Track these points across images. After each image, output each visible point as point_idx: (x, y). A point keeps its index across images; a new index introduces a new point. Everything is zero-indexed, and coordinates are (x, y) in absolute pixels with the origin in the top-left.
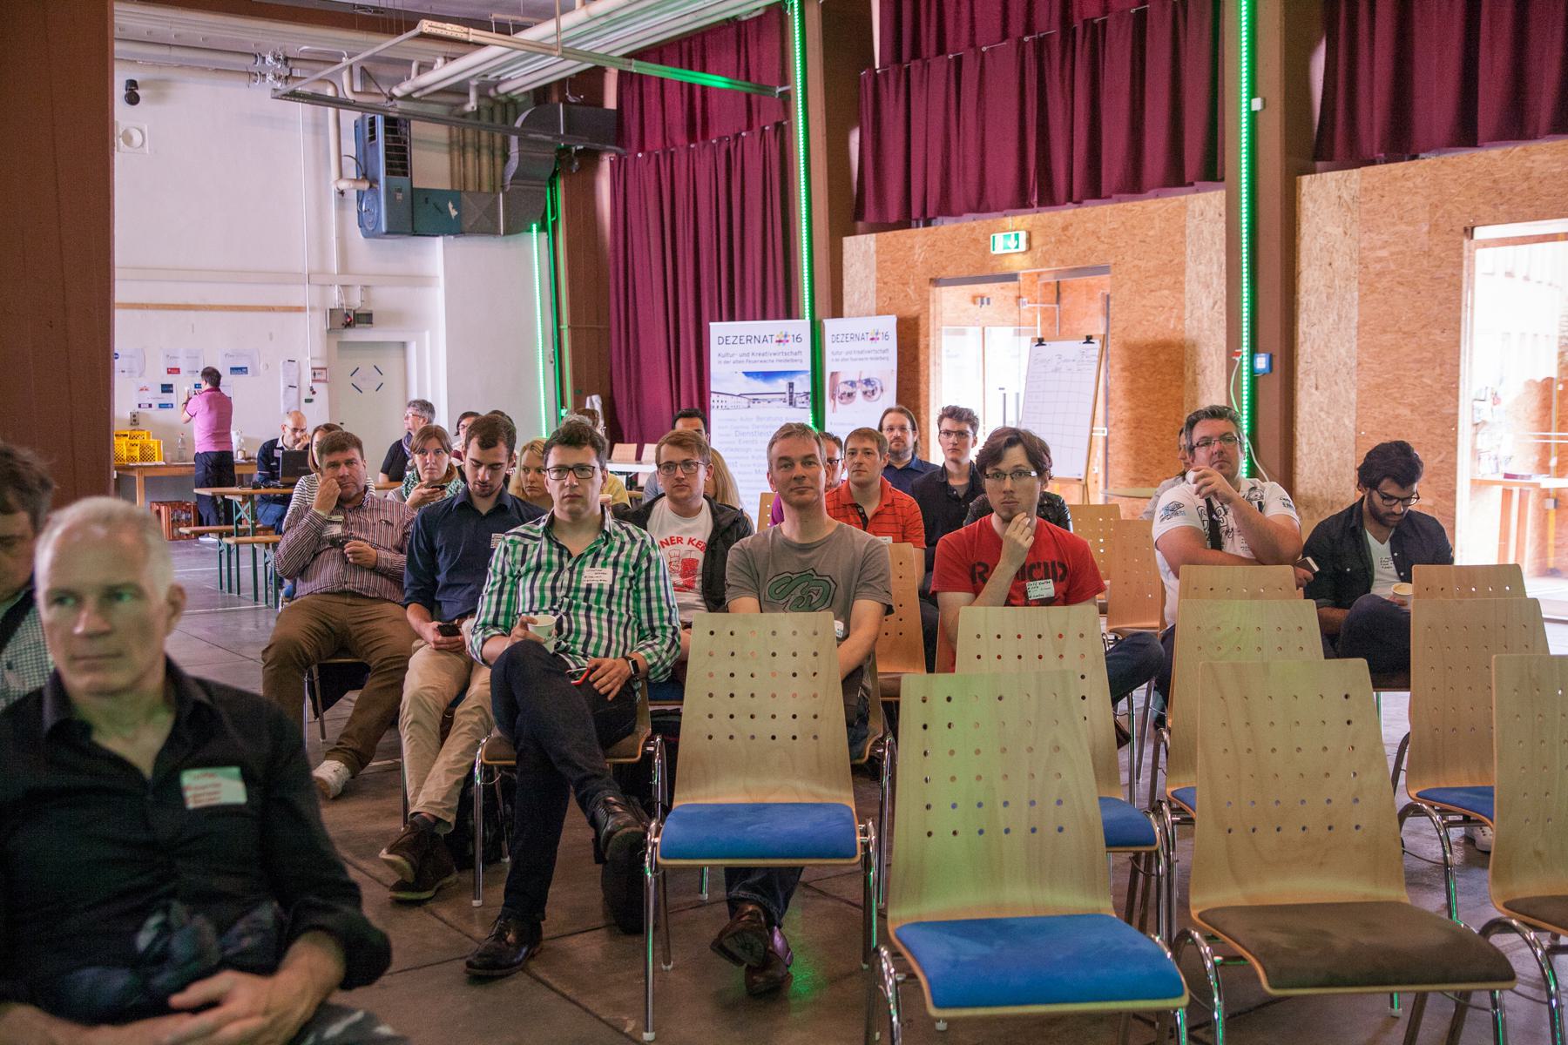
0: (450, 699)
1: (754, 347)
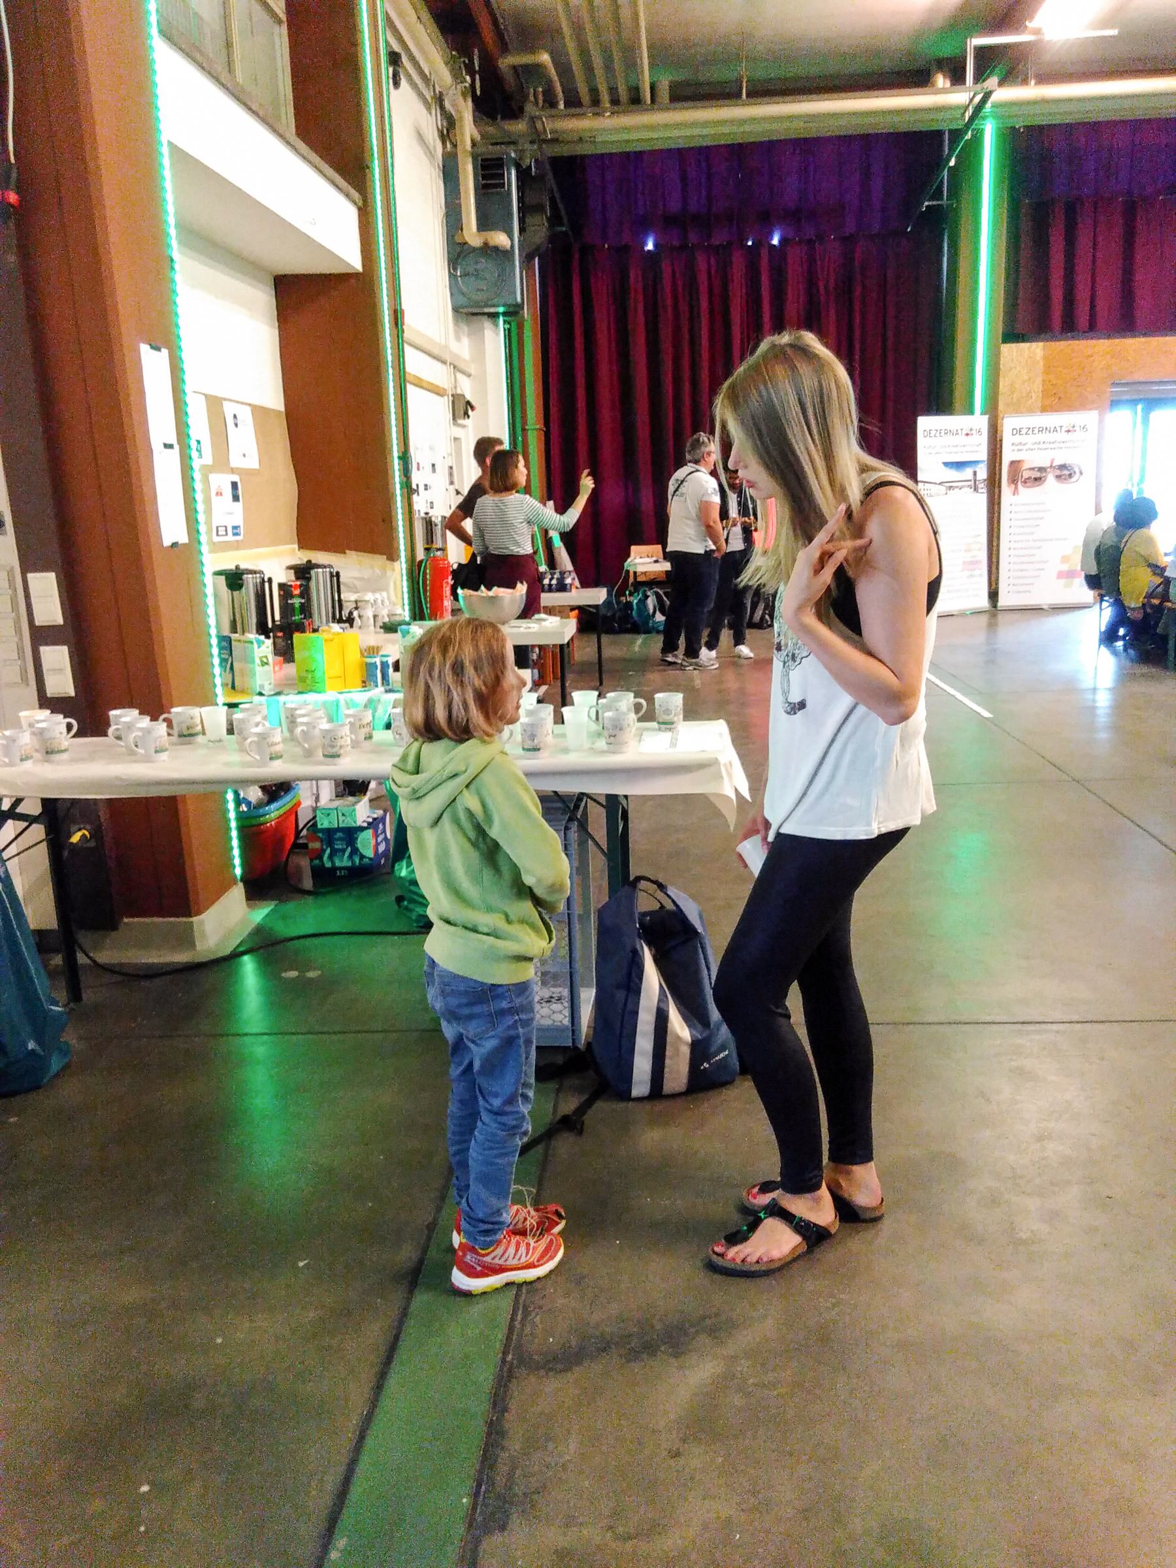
0: (684, 1098)
1: (949, 440)
